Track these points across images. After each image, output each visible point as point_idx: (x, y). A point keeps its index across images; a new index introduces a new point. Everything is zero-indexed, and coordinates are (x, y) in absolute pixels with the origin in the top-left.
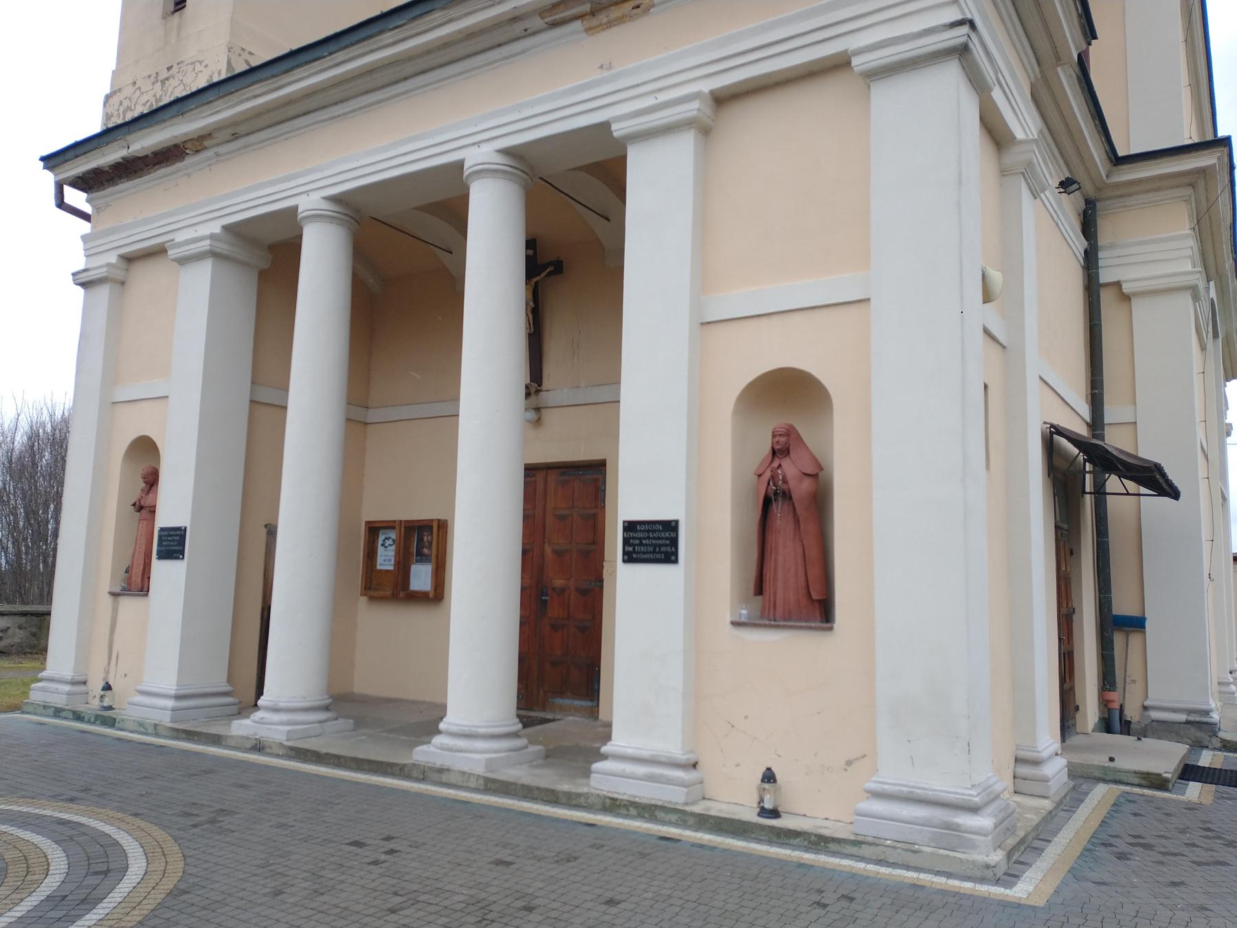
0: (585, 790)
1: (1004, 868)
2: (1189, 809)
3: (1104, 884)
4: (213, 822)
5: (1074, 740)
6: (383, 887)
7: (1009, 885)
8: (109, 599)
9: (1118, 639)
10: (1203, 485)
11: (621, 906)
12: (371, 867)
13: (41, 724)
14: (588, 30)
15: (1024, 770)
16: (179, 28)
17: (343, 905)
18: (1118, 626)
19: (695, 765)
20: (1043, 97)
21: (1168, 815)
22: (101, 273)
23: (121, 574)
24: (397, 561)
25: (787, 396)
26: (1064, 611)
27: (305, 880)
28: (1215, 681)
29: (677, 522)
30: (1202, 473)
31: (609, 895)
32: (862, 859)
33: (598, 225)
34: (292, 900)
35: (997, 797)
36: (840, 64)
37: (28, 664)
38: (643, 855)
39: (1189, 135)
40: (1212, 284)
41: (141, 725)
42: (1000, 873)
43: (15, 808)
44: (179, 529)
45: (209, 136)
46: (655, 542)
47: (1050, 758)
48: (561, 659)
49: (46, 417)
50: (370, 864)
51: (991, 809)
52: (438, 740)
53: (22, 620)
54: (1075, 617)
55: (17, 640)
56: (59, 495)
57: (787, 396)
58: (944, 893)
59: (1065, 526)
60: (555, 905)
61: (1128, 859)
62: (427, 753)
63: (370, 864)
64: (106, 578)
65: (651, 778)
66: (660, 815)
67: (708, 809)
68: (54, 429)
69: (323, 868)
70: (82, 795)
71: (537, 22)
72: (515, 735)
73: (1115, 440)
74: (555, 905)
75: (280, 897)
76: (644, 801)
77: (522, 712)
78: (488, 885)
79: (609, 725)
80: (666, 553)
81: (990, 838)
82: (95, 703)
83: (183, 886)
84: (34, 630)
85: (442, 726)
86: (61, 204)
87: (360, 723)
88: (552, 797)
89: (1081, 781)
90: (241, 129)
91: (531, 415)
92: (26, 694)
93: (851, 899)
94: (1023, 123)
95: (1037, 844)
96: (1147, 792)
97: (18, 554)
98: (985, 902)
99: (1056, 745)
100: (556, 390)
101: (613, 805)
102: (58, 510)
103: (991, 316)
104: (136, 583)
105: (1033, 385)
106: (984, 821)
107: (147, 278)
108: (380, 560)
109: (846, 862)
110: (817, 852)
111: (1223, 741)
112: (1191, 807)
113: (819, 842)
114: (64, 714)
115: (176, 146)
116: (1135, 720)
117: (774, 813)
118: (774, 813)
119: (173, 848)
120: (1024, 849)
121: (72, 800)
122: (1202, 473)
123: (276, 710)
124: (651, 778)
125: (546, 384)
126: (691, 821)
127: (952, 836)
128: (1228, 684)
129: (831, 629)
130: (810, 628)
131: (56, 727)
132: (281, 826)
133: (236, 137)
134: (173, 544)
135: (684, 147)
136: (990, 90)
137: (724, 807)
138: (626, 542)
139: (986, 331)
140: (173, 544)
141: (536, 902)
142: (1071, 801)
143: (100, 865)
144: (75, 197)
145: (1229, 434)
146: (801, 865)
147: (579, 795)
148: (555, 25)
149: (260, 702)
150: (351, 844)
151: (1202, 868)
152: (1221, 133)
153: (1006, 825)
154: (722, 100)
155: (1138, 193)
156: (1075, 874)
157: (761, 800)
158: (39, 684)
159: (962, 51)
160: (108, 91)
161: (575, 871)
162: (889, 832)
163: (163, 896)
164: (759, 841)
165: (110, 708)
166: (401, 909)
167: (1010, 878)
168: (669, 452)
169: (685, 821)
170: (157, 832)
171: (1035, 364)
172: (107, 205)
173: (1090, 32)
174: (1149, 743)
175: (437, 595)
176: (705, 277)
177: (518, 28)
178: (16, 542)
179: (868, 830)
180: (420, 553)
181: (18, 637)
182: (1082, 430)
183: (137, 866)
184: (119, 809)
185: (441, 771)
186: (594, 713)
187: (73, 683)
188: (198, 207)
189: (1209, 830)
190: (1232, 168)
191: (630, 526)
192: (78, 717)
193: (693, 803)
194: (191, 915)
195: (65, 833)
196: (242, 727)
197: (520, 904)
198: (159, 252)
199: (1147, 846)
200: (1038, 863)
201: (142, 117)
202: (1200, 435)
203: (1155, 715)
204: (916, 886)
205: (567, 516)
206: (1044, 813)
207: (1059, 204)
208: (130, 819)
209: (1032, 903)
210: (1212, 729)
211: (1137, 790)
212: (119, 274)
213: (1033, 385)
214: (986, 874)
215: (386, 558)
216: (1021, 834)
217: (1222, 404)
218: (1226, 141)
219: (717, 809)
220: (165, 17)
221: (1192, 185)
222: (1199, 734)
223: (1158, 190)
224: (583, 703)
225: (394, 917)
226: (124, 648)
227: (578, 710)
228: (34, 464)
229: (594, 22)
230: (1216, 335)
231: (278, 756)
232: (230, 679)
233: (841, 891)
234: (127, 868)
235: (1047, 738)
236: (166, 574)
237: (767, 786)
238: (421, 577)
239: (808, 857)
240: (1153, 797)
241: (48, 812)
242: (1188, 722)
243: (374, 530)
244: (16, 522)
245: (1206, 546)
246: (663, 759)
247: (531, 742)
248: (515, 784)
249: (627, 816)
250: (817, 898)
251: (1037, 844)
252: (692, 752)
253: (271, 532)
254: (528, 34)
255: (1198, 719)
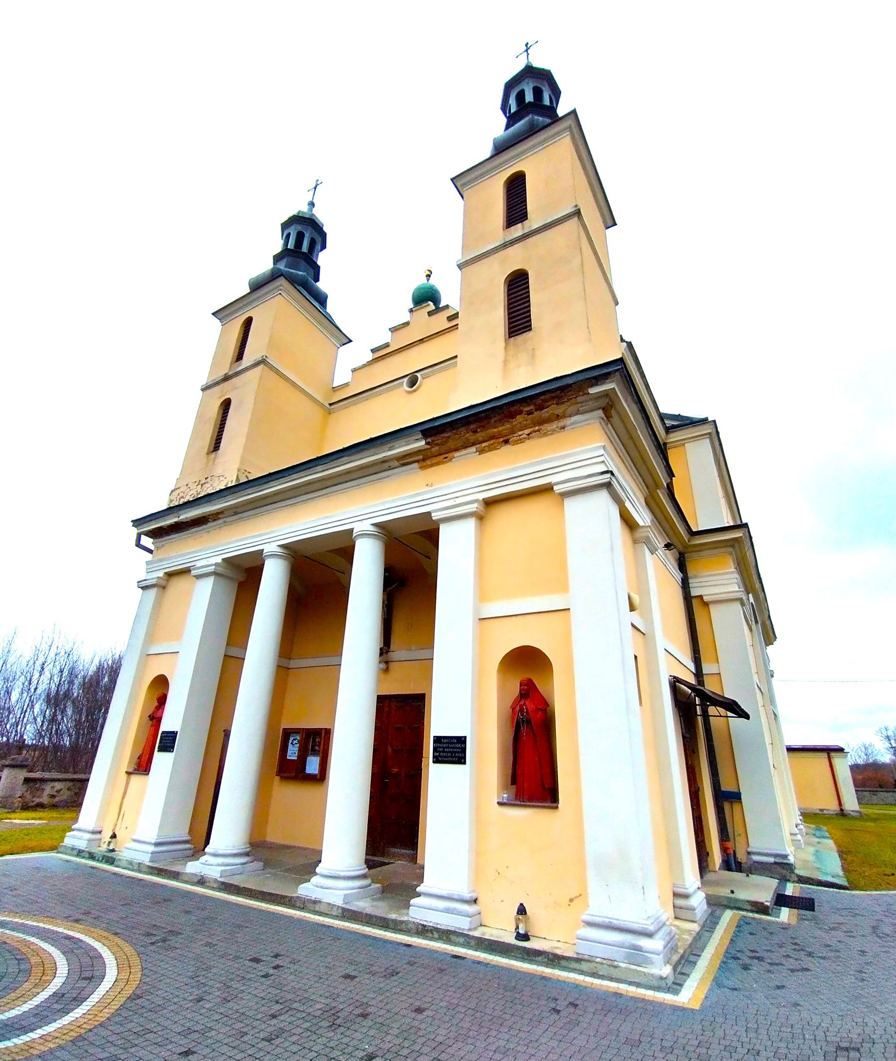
0: (405, 918)
1: (671, 979)
2: (783, 929)
3: (736, 989)
4: (164, 940)
5: (709, 876)
6: (269, 996)
7: (676, 992)
8: (125, 776)
9: (727, 806)
10: (761, 709)
11: (425, 1013)
12: (264, 979)
13: (68, 861)
14: (421, 468)
15: (680, 902)
16: (215, 458)
17: (241, 1011)
18: (727, 798)
19: (475, 901)
20: (651, 503)
21: (771, 933)
22: (154, 582)
23: (136, 760)
24: (298, 755)
25: (527, 663)
26: (693, 789)
27: (219, 990)
28: (788, 834)
29: (465, 737)
30: (760, 703)
31: (417, 1004)
32: (582, 972)
33: (424, 560)
34: (207, 1006)
35: (664, 924)
36: (547, 489)
37: (68, 815)
38: (441, 971)
39: (728, 522)
40: (750, 595)
41: (131, 863)
42: (670, 982)
43: (41, 925)
44: (173, 732)
45: (222, 512)
46: (452, 750)
47: (695, 892)
48: (395, 824)
49: (110, 656)
50: (263, 976)
51: (660, 934)
52: (315, 880)
53: (70, 784)
54: (700, 793)
55: (65, 797)
56: (108, 702)
57: (527, 663)
58: (635, 999)
59: (688, 736)
60: (382, 1012)
61: (749, 969)
62: (306, 890)
63: (263, 976)
64: (125, 764)
65: (447, 911)
66: (453, 938)
67: (484, 934)
68: (113, 662)
69: (231, 980)
70: (84, 917)
71: (396, 463)
72: (364, 876)
73: (710, 686)
74: (382, 1012)
75: (200, 1003)
76: (443, 927)
77: (369, 857)
78: (338, 995)
79: (423, 867)
80: (459, 757)
81: (662, 956)
82: (104, 847)
83: (138, 992)
84: (77, 791)
85: (318, 870)
86: (138, 544)
87: (267, 864)
88: (384, 923)
89: (715, 908)
90: (238, 510)
91: (383, 666)
92: (62, 838)
93: (576, 1006)
94: (643, 517)
95: (692, 958)
96: (757, 916)
97: (77, 739)
98: (661, 1006)
99: (698, 883)
100: (397, 653)
101: (423, 931)
102: (106, 712)
103: (635, 618)
104: (143, 766)
105: (662, 656)
106: (656, 944)
107: (178, 585)
108: (289, 752)
109: (572, 975)
110: (554, 967)
111: (798, 876)
112: (785, 927)
113: (554, 959)
114: (82, 854)
115: (204, 517)
116: (744, 861)
117: (525, 937)
118: (525, 937)
119: (135, 960)
120: (684, 962)
121: (77, 921)
122: (760, 703)
123: (215, 855)
124: (447, 911)
125: (392, 647)
126: (473, 943)
127: (637, 954)
128: (796, 834)
129: (557, 808)
130: (544, 807)
131: (77, 864)
132: (208, 944)
133: (236, 513)
134: (168, 742)
135: (470, 524)
136: (624, 503)
137: (495, 932)
138: (435, 749)
139: (633, 625)
140: (168, 742)
141: (369, 1010)
142: (710, 924)
143: (87, 971)
144: (147, 541)
145: (772, 676)
146: (544, 978)
147: (402, 922)
148: (404, 465)
149: (206, 850)
150: (251, 960)
151: (796, 974)
152: (744, 521)
153: (671, 946)
154: (489, 503)
155: (706, 550)
156: (717, 983)
157: (517, 928)
158: (72, 833)
159: (608, 486)
160: (173, 488)
161: (395, 984)
162: (598, 952)
163: (124, 999)
164: (516, 958)
165: (113, 850)
166: (280, 1015)
167: (676, 987)
168: (462, 699)
169: (469, 943)
170: (129, 950)
171: (661, 642)
172: (163, 546)
173: (671, 474)
174: (755, 878)
175: (321, 777)
176: (482, 594)
177: (386, 465)
178: (78, 734)
179: (585, 950)
180: (313, 750)
181: (65, 795)
182: (692, 680)
183: (111, 974)
184: (107, 930)
185: (315, 902)
186: (414, 858)
187: (93, 833)
188: (210, 550)
189: (796, 944)
190: (751, 538)
191: (438, 739)
192: (92, 856)
193: (475, 929)
194: (141, 1015)
195: (70, 946)
196: (193, 867)
197: (358, 1011)
198: (186, 571)
199: (760, 959)
200: (693, 974)
201: (189, 502)
202: (756, 678)
203: (756, 858)
204: (618, 995)
205: (401, 724)
206: (694, 934)
207: (666, 556)
208: (111, 937)
209: (691, 1007)
210: (790, 867)
211: (750, 915)
212: (163, 583)
213: (662, 656)
214: (660, 985)
215: (293, 752)
216: (681, 951)
217: (766, 660)
218: (747, 524)
219: (490, 934)
220: (208, 454)
221: (733, 546)
222: (784, 872)
223: (717, 548)
224: (407, 851)
225: (274, 1021)
226: (127, 811)
227: (401, 857)
228: (98, 683)
229: (424, 464)
230: (756, 622)
231: (213, 889)
232: (191, 832)
233: (571, 1000)
234: (104, 977)
235: (691, 878)
236: (162, 761)
237: (520, 917)
238: (313, 765)
239: (548, 971)
240: (760, 919)
241: (60, 930)
242: (776, 863)
243: (287, 733)
244: (80, 718)
245: (769, 747)
246: (455, 897)
247: (373, 882)
248: (361, 913)
249: (431, 939)
250: (553, 1005)
251: (692, 958)
252: (474, 891)
253: (227, 734)
254: (390, 468)
255: (781, 861)
